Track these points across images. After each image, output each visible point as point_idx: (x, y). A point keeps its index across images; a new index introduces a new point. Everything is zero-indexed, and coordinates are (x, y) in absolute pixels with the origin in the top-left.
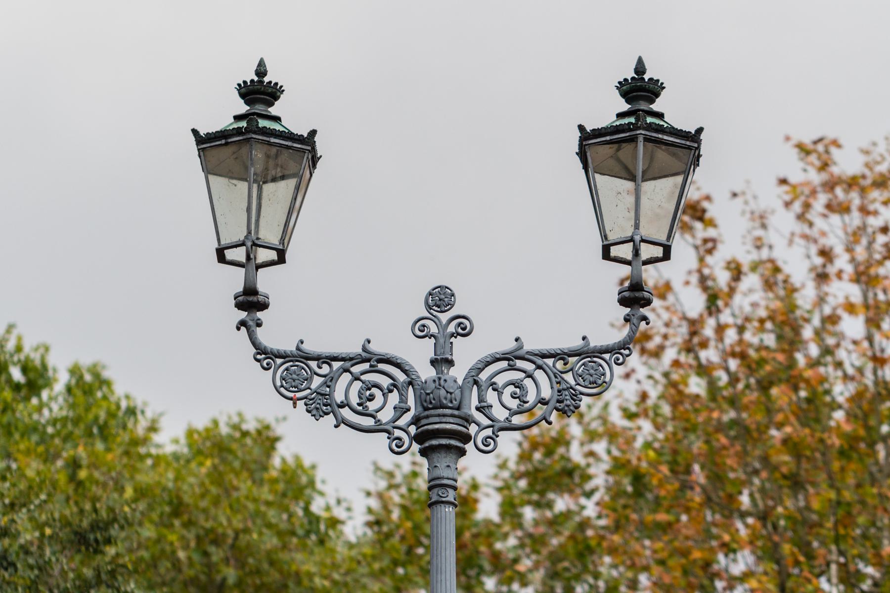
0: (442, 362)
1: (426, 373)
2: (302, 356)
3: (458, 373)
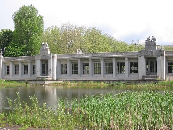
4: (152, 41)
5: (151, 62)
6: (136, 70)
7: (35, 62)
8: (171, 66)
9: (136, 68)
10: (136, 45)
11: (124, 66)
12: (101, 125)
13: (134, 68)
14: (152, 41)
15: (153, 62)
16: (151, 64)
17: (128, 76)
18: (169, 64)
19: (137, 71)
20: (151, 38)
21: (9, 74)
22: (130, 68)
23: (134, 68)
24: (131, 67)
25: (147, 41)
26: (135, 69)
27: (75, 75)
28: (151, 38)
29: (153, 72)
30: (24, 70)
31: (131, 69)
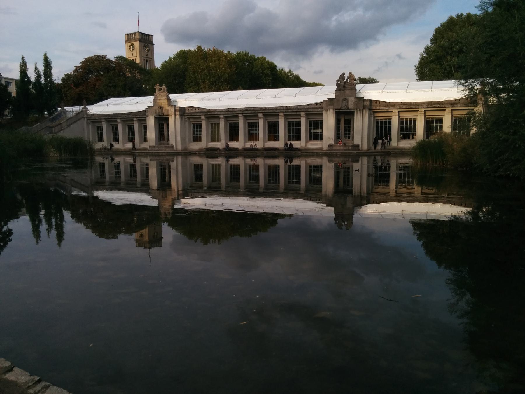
4: (349, 81)
5: (346, 120)
7: (145, 120)
15: (163, 125)
20: (346, 76)
25: (339, 82)
28: (346, 76)
31: (310, 132)
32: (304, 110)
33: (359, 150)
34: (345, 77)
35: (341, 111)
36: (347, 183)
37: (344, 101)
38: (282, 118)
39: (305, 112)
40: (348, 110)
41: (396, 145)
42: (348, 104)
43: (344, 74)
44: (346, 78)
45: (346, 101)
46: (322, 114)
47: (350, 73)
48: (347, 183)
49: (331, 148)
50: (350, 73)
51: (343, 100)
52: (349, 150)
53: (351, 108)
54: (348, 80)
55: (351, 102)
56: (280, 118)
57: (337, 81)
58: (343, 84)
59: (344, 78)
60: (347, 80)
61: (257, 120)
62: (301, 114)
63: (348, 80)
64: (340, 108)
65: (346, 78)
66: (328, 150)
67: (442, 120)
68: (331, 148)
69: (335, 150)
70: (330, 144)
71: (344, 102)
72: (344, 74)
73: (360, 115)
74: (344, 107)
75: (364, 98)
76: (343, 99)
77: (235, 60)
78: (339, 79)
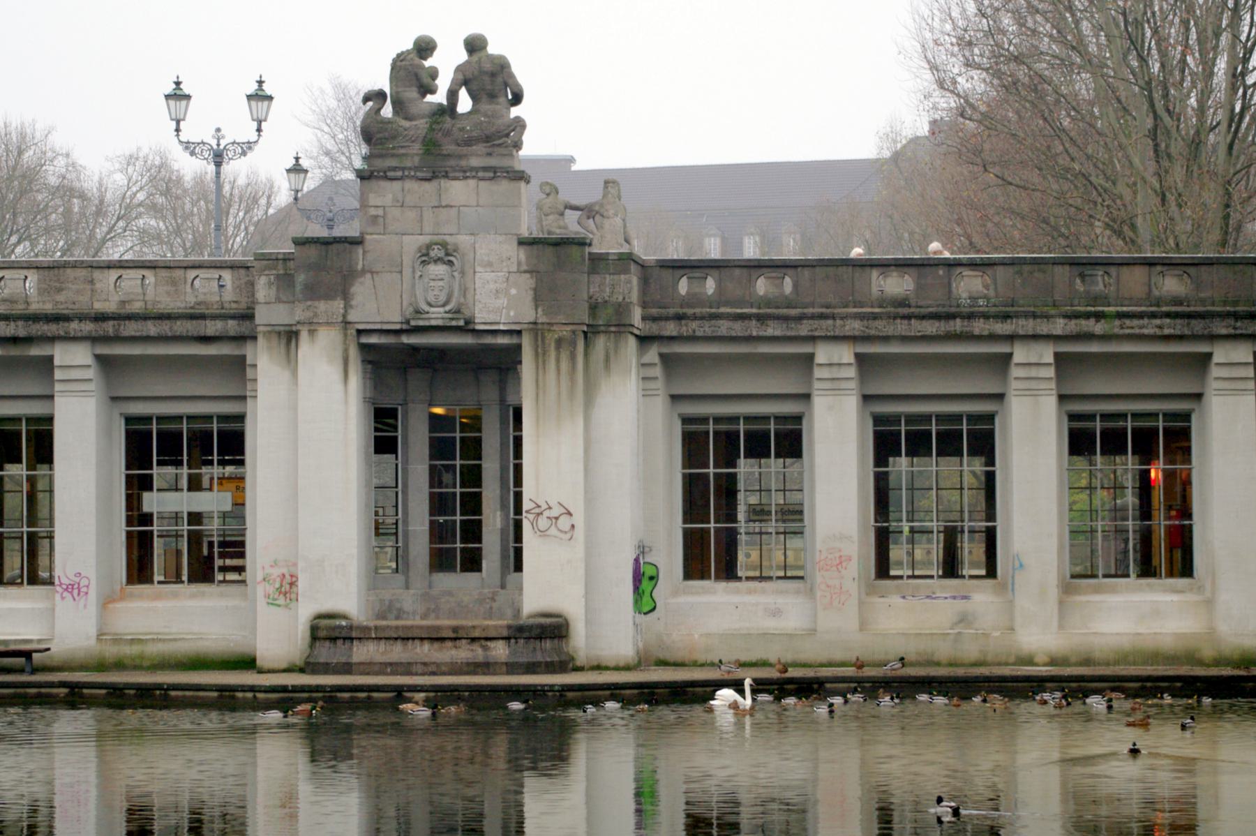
0: (218, 145)
1: (215, 147)
2: (188, 142)
3: (222, 147)
4: (465, 103)
6: (213, 527)
8: (728, 489)
9: (212, 502)
10: (218, 158)
11: (42, 471)
12: (1157, 65)
13: (185, 502)
14: (465, 103)
16: (440, 449)
17: (497, 581)
18: (693, 445)
19: (235, 547)
21: (1183, 566)
22: (133, 502)
23: (185, 502)
24: (138, 485)
25: (387, 111)
26: (195, 518)
27: (456, 583)
29: (472, 562)
30: (770, 578)
31: (137, 517)
32: (88, 327)
33: (565, 665)
34: (434, 74)
35: (405, 339)
36: (965, 427)
37: (438, 260)
38: (1043, 385)
39: (94, 340)
40: (468, 340)
41: (854, 624)
42: (464, 291)
43: (425, 48)
44: (444, 83)
45: (450, 263)
46: (239, 366)
47: (474, 45)
48: (965, 427)
49: (325, 653)
50: (474, 45)
51: (425, 256)
52: (485, 667)
53: (491, 318)
54: (463, 95)
55: (490, 276)
56: (817, 385)
57: (366, 99)
58: (422, 124)
59: (426, 80)
60: (453, 95)
61: (873, 390)
62: (57, 362)
63: (463, 95)
64: (398, 318)
65: (444, 83)
66: (307, 667)
67: (1185, 434)
68: (325, 653)
69: (368, 667)
70: (320, 616)
71: (439, 270)
72: (425, 48)
73: (564, 365)
74: (437, 316)
75: (571, 160)
76: (429, 247)
77: (971, 769)
78: (387, 90)
